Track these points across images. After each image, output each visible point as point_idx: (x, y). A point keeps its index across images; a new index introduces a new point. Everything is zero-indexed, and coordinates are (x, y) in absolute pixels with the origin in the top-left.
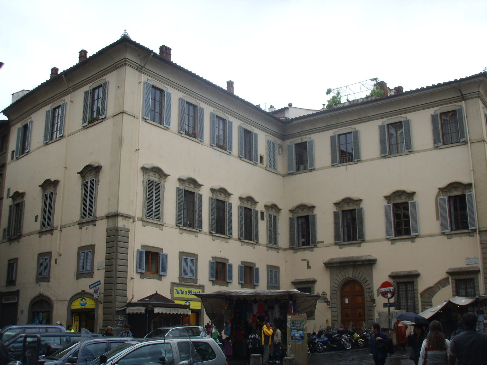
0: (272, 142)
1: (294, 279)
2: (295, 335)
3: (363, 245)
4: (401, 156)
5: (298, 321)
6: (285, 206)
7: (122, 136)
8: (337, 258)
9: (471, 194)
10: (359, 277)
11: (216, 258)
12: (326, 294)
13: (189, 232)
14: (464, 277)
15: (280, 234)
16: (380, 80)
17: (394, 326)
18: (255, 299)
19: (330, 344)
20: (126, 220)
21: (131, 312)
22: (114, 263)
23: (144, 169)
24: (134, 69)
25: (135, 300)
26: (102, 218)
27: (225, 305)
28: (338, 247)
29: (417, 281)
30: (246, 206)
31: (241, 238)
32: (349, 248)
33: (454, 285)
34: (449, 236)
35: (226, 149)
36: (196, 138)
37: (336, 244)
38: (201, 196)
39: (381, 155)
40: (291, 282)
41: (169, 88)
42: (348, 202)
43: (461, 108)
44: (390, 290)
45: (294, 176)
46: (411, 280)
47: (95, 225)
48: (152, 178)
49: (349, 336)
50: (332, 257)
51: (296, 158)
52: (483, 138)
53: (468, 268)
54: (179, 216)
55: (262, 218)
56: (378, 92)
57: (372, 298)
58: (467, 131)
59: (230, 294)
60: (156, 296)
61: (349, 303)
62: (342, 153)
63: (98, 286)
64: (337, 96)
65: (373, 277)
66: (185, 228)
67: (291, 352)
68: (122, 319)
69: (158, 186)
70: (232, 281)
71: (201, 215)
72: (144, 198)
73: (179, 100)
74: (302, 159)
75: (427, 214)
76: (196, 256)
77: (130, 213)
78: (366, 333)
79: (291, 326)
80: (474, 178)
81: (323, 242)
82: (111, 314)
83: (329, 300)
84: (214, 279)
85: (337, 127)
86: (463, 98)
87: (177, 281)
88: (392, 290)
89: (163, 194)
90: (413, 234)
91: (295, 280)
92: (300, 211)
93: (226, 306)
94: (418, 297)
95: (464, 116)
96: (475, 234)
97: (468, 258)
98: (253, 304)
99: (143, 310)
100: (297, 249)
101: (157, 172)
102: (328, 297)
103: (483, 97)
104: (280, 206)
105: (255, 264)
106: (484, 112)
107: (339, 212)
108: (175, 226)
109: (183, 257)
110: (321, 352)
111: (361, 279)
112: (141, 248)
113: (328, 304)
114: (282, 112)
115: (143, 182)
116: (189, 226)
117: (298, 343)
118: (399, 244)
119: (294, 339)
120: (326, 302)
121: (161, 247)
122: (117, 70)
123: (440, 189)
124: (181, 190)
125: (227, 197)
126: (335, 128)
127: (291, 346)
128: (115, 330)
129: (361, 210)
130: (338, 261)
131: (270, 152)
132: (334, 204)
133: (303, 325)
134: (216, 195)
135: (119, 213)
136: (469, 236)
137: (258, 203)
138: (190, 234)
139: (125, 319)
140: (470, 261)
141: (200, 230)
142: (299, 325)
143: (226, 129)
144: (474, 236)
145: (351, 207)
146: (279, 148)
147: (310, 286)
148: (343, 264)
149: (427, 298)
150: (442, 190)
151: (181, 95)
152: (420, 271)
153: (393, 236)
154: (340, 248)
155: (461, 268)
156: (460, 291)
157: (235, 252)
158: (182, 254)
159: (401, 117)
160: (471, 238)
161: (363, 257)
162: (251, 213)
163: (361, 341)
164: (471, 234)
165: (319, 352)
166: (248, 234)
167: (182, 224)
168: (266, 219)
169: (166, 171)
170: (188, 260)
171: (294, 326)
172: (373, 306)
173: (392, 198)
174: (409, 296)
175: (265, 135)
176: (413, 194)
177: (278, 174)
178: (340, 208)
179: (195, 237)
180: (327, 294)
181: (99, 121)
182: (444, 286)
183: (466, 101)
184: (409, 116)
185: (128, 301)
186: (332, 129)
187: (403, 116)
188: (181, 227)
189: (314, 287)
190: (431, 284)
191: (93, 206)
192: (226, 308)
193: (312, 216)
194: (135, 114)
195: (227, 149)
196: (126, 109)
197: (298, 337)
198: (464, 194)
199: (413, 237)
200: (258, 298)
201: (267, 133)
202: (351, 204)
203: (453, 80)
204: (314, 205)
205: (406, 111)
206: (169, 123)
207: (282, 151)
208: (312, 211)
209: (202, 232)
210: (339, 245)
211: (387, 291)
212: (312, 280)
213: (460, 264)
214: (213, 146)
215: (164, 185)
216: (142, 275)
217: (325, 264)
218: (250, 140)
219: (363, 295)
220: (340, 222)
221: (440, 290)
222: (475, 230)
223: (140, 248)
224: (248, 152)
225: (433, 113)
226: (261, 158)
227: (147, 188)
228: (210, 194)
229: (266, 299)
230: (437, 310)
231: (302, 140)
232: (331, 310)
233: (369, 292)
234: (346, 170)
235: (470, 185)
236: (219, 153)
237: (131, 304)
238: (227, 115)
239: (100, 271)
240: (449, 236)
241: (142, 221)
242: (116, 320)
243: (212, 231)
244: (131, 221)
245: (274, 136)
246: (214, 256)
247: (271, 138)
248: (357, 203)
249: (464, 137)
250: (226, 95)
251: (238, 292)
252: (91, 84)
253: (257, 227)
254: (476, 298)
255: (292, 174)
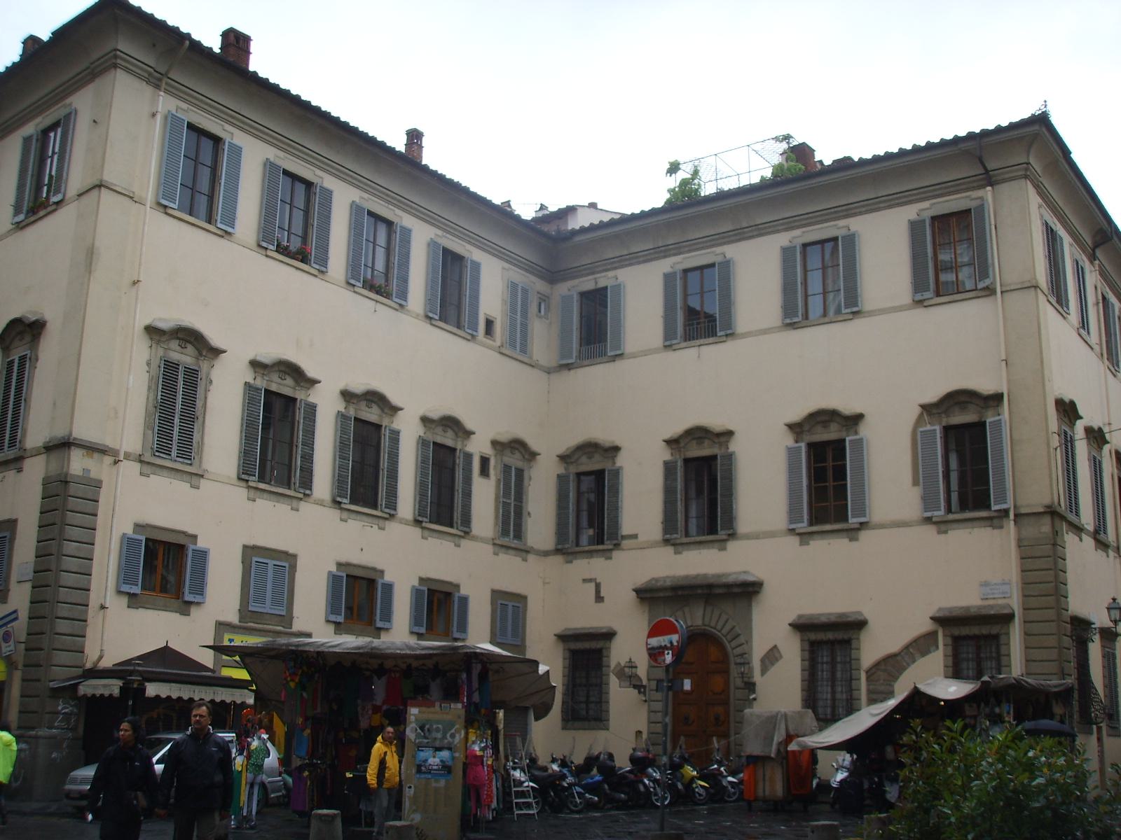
0: (520, 285)
1: (563, 628)
2: (427, 760)
3: (731, 545)
4: (830, 323)
5: (438, 722)
6: (550, 445)
7: (93, 244)
8: (667, 577)
9: (1000, 420)
10: (719, 627)
11: (348, 565)
12: (636, 667)
13: (273, 497)
14: (975, 630)
15: (532, 515)
16: (798, 140)
17: (779, 751)
18: (381, 665)
19: (608, 792)
20: (92, 458)
21: (89, 692)
22: (53, 567)
23: (152, 331)
24: (138, 80)
25: (107, 663)
26: (36, 453)
27: (289, 679)
28: (670, 549)
29: (858, 639)
30: (439, 440)
31: (420, 519)
32: (699, 551)
33: (950, 652)
34: (942, 525)
35: (392, 295)
36: (306, 264)
37: (666, 542)
38: (312, 409)
39: (783, 320)
40: (555, 635)
41: (236, 132)
42: (700, 438)
43: (983, 205)
44: (671, 643)
46: (846, 637)
47: (20, 470)
48: (175, 356)
49: (669, 774)
50: (656, 576)
51: (581, 328)
52: (1035, 279)
53: (985, 607)
54: (246, 454)
55: (484, 472)
56: (789, 169)
57: (746, 679)
58: (996, 261)
59: (300, 648)
60: (166, 655)
61: (692, 691)
62: (691, 314)
63: (13, 624)
64: (693, 179)
65: (754, 627)
66: (262, 486)
67: (414, 808)
68: (66, 710)
69: (192, 377)
70: (391, 624)
71: (311, 456)
72: (151, 405)
73: (265, 165)
74: (594, 332)
75: (890, 470)
76: (291, 558)
77: (109, 442)
78: (716, 766)
79: (418, 736)
80: (1009, 381)
81: (635, 536)
82: (38, 696)
83: (645, 682)
84: (423, 630)
85: (682, 250)
86: (989, 179)
87: (233, 617)
88: (675, 644)
89: (206, 398)
90: (853, 521)
91: (566, 629)
92: (584, 459)
93: (292, 680)
94: (859, 679)
95: (990, 225)
96: (1005, 521)
97: (985, 582)
98: (375, 678)
99: (115, 687)
100: (572, 553)
101: (192, 340)
102: (642, 671)
103: (1040, 179)
104: (534, 445)
105: (457, 586)
106: (1042, 216)
107: (676, 462)
108: (235, 481)
109: (255, 559)
110: (578, 812)
111: (724, 631)
112: (420, 584)
113: (640, 692)
114: (560, 218)
115: (148, 364)
116: (276, 482)
117: (434, 784)
118: (819, 546)
119: (424, 773)
120: (635, 687)
121: (191, 531)
122: (97, 81)
123: (923, 407)
124: (258, 389)
125: (386, 413)
126: (675, 255)
127: (415, 792)
128: (46, 738)
129: (730, 457)
130: (668, 583)
131: (513, 310)
132: (665, 441)
133: (453, 736)
134: (356, 409)
135: (72, 438)
136: (990, 526)
137: (474, 433)
138: (278, 502)
139: (75, 710)
140: (991, 589)
141: (305, 494)
142: (439, 735)
143: (392, 246)
144: (1001, 527)
145: (705, 451)
146: (540, 303)
148: (680, 593)
149: (882, 681)
150: (928, 409)
151: (271, 153)
152: (867, 613)
153: (805, 524)
154: (675, 553)
155: (968, 608)
156: (964, 665)
157: (403, 553)
158: (250, 552)
159: (835, 225)
160: (996, 532)
161: (729, 575)
162: (454, 456)
163: (701, 785)
164: (995, 521)
165: (573, 812)
166: (443, 508)
167: (255, 476)
168: (496, 475)
169: (215, 339)
170: (268, 569)
171: (425, 737)
172: (748, 700)
173: (806, 428)
174: (839, 675)
175: (503, 268)
176: (857, 419)
177: (533, 366)
178: (680, 451)
179: (292, 509)
180: (638, 666)
181: (50, 209)
182: (924, 653)
183: (996, 187)
184: (856, 224)
185: (89, 665)
186: (669, 256)
187: (842, 223)
188: (251, 484)
189: (610, 648)
190: (894, 646)
191: (21, 421)
192: (292, 684)
193: (612, 470)
194: (134, 193)
195: (394, 295)
196: (108, 177)
197: (435, 767)
198: (983, 420)
199: (852, 526)
200: (388, 664)
201: (510, 263)
202: (707, 442)
203: (962, 133)
204: (618, 443)
205: (849, 211)
206: (231, 219)
207: (548, 309)
208: (614, 460)
209: (311, 499)
210: (674, 545)
211: (663, 644)
212: (604, 631)
213: (967, 598)
214: (354, 286)
215: (208, 374)
216: (134, 601)
217: (638, 591)
218: (461, 277)
219: (726, 672)
220: (679, 487)
221: (916, 663)
222: (1006, 512)
223: (129, 531)
224: (452, 302)
225: (913, 216)
226: (489, 324)
227: (161, 380)
228: (340, 406)
229: (409, 666)
230: (882, 713)
231: (596, 283)
232: (649, 706)
233: (740, 664)
234: (699, 357)
235: (997, 398)
237: (95, 673)
238: (469, 247)
239: (23, 584)
240: (943, 527)
241: (141, 462)
242: (47, 713)
243: (340, 496)
244: (108, 460)
245: (526, 270)
246: (343, 559)
247: (519, 276)
248: (722, 439)
249: (988, 277)
250: (404, 165)
251: (323, 645)
252: (39, 119)
253: (468, 495)
254: (983, 682)
255: (568, 367)
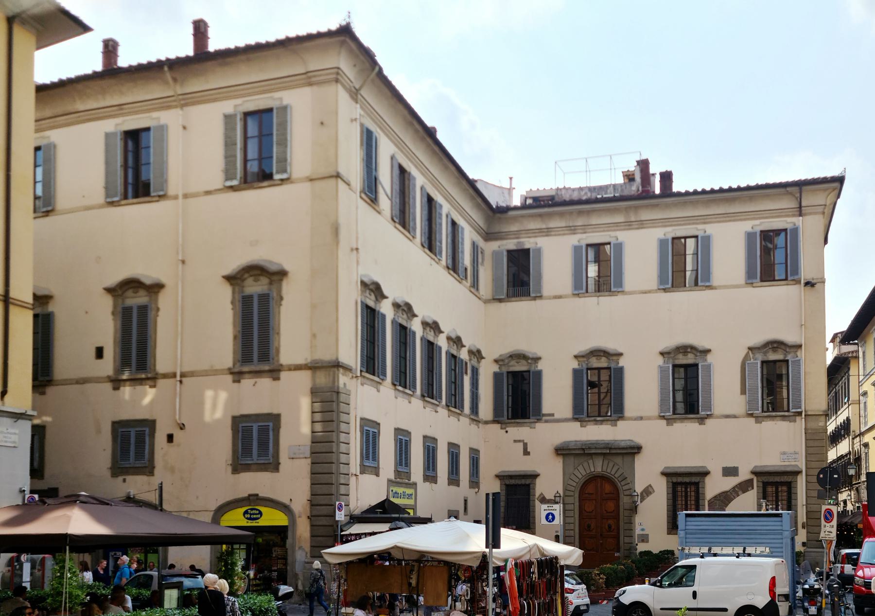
3: (620, 423)
10: (613, 473)
45: (503, 304)
47: (277, 379)
81: (553, 415)
90: (702, 413)
111: (616, 476)
118: (678, 426)
147: (528, 482)
205: (705, 219)
236: (429, 258)
255: (500, 301)
